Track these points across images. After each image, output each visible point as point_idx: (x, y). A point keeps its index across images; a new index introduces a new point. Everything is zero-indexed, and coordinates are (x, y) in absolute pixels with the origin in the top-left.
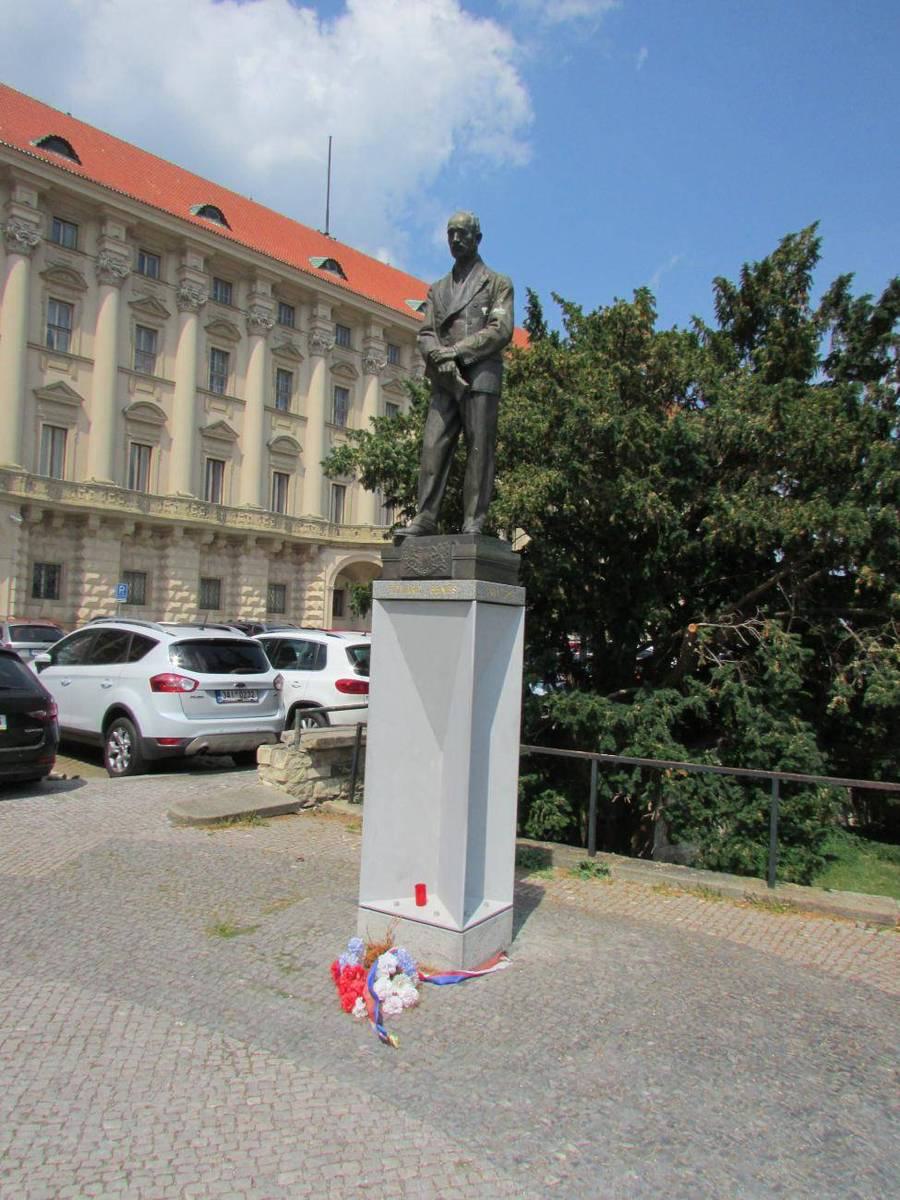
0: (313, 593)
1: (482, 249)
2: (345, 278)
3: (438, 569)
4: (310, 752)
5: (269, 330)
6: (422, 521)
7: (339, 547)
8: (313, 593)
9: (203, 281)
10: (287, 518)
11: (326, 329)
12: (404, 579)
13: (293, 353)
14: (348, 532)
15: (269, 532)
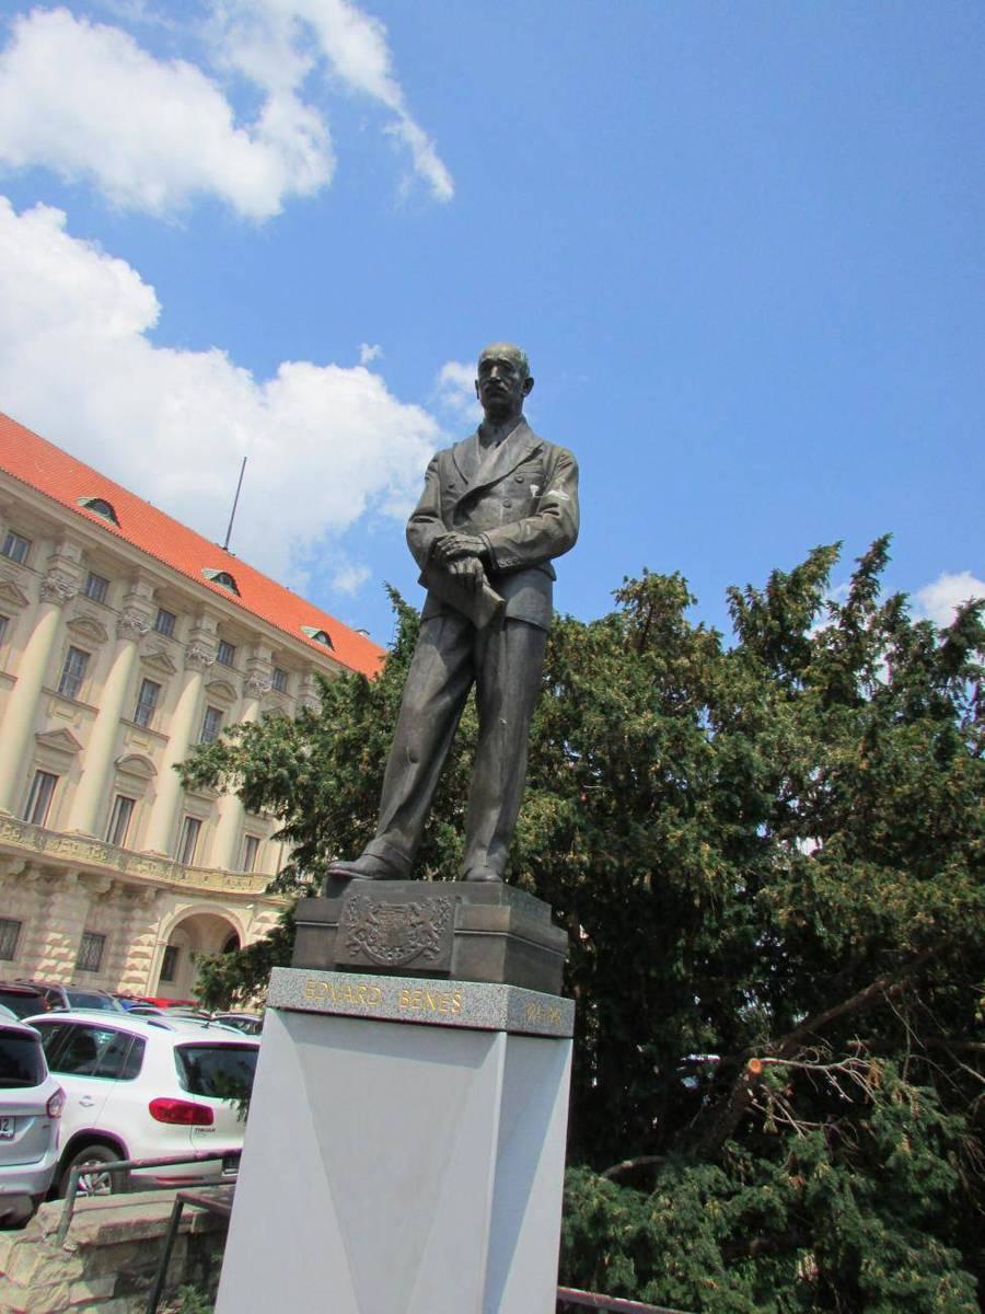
0: (138, 949)
1: (529, 407)
2: (239, 595)
3: (420, 954)
4: (84, 1249)
5: (142, 636)
6: (387, 849)
7: (181, 894)
8: (138, 949)
9: (76, 573)
10: (123, 851)
11: (208, 645)
12: (341, 968)
13: (165, 663)
14: (194, 875)
15: (98, 867)
